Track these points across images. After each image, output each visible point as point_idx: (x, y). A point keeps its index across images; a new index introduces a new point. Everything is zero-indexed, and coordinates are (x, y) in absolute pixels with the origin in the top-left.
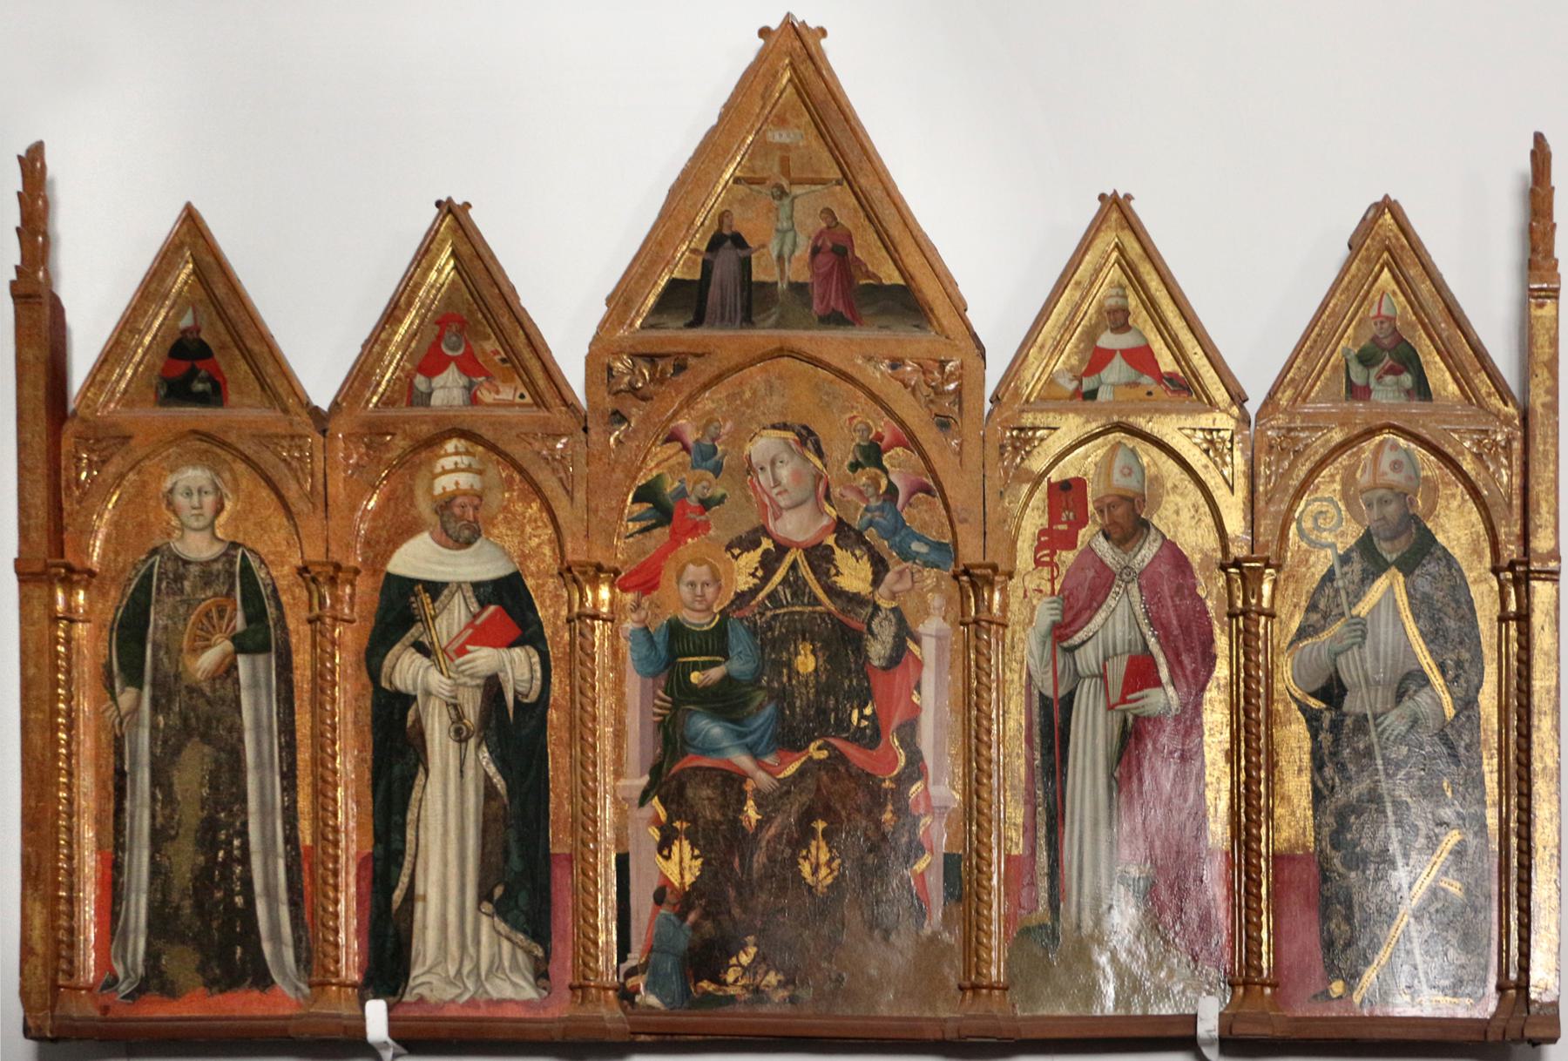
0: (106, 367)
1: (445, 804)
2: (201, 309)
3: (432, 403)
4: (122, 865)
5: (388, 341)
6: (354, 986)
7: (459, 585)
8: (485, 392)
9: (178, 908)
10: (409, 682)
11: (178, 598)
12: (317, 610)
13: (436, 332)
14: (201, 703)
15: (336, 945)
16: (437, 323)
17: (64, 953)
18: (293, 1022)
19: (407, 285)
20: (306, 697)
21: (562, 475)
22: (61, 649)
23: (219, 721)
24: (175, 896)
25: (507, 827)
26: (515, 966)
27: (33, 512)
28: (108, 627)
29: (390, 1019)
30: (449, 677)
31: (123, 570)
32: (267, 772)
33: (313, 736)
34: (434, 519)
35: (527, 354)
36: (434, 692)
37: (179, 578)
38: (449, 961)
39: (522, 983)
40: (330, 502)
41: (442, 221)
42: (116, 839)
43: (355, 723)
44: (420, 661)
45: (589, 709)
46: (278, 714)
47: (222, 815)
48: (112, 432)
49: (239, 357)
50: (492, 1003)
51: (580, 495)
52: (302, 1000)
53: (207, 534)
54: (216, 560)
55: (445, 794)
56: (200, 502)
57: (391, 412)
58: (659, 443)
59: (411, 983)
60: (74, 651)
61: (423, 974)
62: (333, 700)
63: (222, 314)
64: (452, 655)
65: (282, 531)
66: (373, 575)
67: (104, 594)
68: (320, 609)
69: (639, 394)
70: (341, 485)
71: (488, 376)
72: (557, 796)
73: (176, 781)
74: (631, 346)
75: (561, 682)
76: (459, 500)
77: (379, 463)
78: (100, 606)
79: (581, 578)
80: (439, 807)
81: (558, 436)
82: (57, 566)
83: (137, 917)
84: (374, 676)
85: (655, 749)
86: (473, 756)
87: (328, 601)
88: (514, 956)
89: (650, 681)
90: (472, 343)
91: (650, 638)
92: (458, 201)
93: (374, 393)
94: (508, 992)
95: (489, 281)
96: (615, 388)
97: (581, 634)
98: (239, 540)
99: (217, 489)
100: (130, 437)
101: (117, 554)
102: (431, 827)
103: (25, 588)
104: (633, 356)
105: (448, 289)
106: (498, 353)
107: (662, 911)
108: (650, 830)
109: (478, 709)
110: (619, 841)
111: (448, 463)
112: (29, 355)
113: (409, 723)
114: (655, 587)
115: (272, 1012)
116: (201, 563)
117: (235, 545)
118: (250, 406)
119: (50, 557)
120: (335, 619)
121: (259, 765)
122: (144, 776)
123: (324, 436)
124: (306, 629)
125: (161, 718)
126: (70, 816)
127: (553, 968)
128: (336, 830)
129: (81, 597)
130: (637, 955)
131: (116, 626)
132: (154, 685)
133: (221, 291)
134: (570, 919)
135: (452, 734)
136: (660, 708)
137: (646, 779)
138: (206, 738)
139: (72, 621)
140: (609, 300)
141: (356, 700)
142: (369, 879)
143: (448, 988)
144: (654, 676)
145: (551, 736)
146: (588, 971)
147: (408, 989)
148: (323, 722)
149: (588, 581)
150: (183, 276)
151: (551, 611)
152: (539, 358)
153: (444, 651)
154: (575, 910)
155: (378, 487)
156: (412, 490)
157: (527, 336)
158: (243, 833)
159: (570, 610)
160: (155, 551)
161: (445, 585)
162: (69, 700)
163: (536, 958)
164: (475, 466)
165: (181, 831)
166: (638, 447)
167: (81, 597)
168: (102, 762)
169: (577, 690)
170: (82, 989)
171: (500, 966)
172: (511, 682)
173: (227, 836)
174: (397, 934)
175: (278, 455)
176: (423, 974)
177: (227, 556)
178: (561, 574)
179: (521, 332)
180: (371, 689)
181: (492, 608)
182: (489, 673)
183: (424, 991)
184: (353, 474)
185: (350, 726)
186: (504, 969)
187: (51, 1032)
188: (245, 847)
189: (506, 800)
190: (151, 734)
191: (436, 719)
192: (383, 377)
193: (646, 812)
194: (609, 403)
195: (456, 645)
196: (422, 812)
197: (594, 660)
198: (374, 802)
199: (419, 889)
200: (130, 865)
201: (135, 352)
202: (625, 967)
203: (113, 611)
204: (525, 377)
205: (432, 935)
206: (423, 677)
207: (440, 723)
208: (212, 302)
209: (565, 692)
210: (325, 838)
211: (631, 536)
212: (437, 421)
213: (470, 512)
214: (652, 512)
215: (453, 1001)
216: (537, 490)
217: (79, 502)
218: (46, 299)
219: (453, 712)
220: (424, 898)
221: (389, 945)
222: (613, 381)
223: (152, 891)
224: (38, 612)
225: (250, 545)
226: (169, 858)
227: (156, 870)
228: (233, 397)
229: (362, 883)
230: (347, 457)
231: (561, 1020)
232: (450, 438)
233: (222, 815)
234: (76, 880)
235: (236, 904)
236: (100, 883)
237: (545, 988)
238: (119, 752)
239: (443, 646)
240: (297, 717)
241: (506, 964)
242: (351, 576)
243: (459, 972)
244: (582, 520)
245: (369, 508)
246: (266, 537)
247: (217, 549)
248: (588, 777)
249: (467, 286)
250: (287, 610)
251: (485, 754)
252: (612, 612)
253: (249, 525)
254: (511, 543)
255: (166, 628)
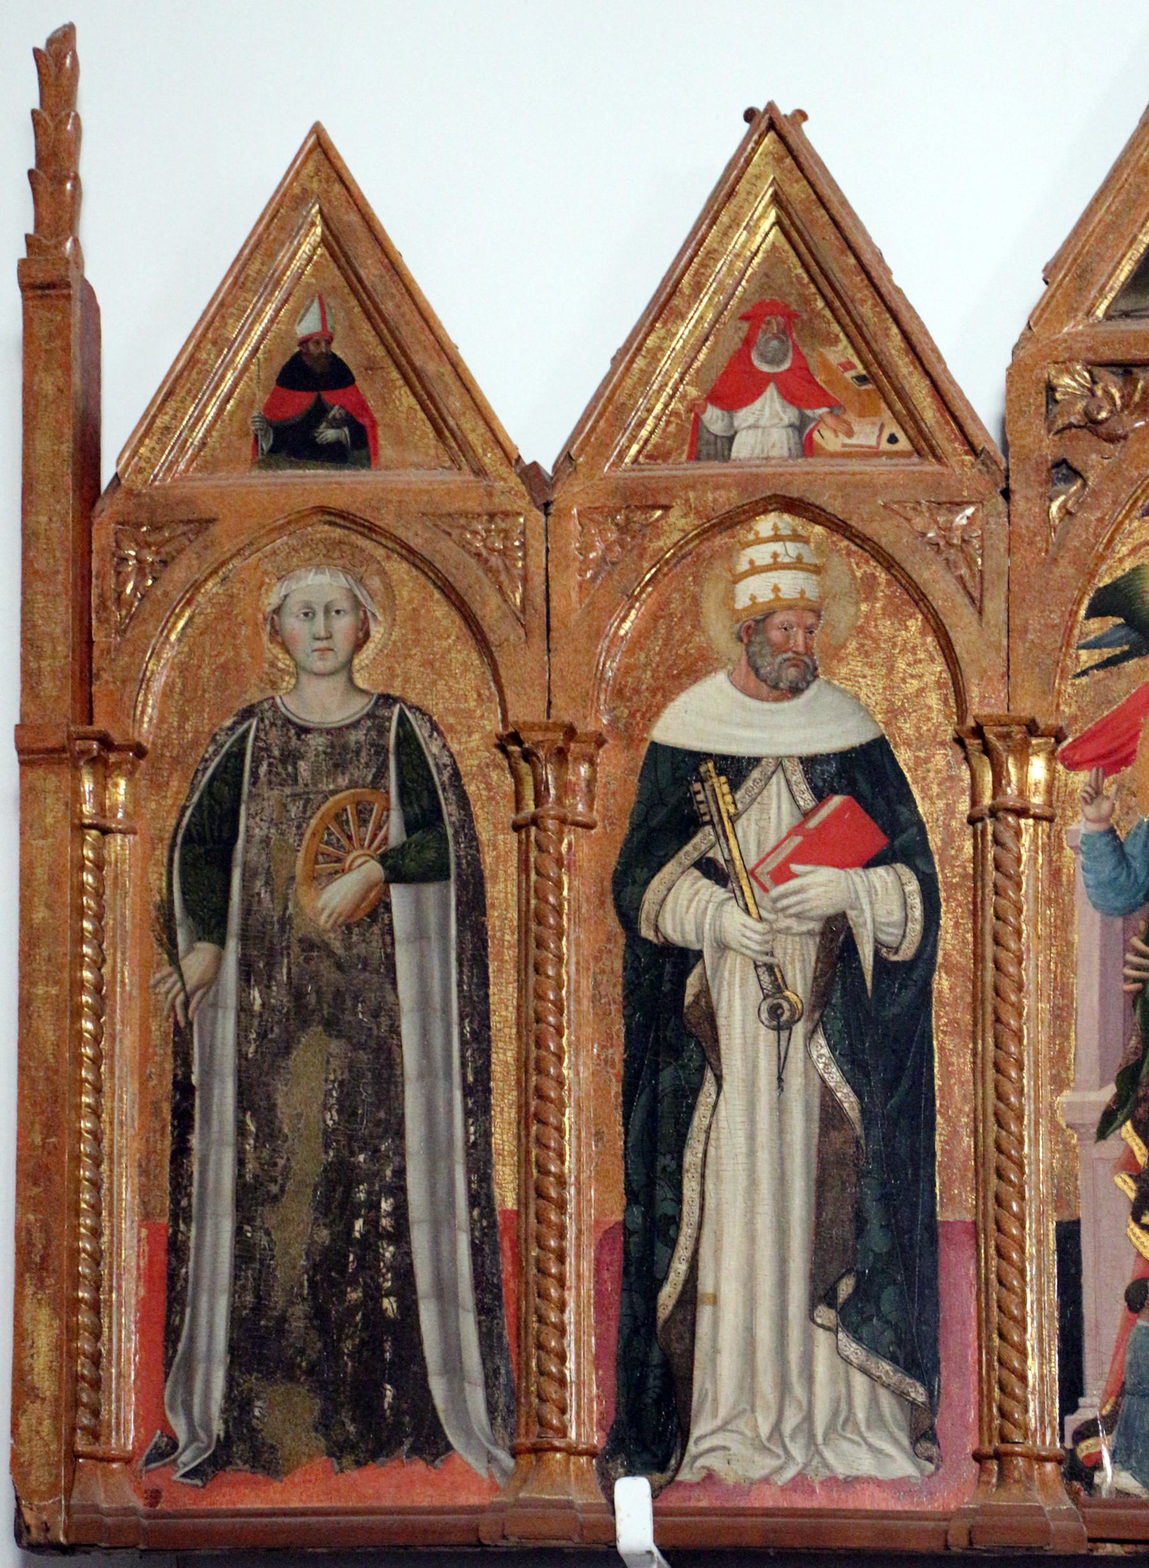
0: (172, 405)
1: (752, 1137)
2: (330, 301)
3: (734, 454)
4: (185, 1243)
5: (654, 357)
6: (591, 1453)
7: (779, 762)
8: (827, 433)
9: (283, 1319)
10: (690, 928)
11: (288, 791)
12: (530, 807)
13: (742, 335)
14: (325, 968)
15: (562, 1382)
16: (745, 318)
17: (85, 1398)
18: (489, 1516)
19: (695, 254)
20: (510, 954)
21: (964, 571)
22: (88, 878)
23: (356, 998)
24: (278, 1298)
25: (861, 1174)
26: (876, 1419)
27: (47, 647)
28: (167, 842)
29: (657, 1513)
30: (761, 919)
31: (195, 744)
32: (441, 1084)
33: (521, 1024)
34: (737, 651)
35: (903, 366)
36: (734, 945)
37: (290, 757)
38: (759, 1410)
39: (888, 1448)
40: (554, 623)
41: (758, 143)
42: (176, 1202)
43: (594, 999)
44: (708, 889)
45: (1012, 970)
46: (460, 984)
47: (361, 1158)
48: (183, 513)
49: (401, 382)
50: (832, 1482)
51: (995, 606)
52: (499, 1480)
53: (340, 680)
54: (355, 725)
55: (752, 1121)
56: (328, 627)
57: (661, 470)
58: (1136, 513)
59: (692, 1448)
60: (109, 883)
61: (713, 1432)
62: (559, 958)
63: (373, 313)
64: (767, 880)
65: (470, 675)
66: (628, 747)
67: (158, 786)
68: (537, 806)
69: (1102, 429)
70: (574, 595)
71: (833, 405)
72: (948, 1120)
73: (280, 1101)
74: (1089, 349)
75: (957, 925)
76: (779, 618)
77: (641, 556)
78: (153, 806)
79: (999, 745)
80: (741, 1140)
81: (958, 505)
82: (85, 737)
83: (211, 1336)
84: (628, 918)
85: (1127, 1038)
86: (801, 1055)
87: (552, 791)
88: (874, 1401)
89: (1119, 923)
90: (805, 351)
91: (1118, 848)
92: (786, 109)
93: (633, 439)
94: (866, 1465)
95: (837, 243)
96: (1060, 423)
97: (997, 841)
98: (396, 692)
99: (357, 604)
100: (212, 521)
101: (184, 717)
102: (726, 1175)
103: (31, 775)
104: (1093, 365)
105: (764, 260)
106: (853, 367)
107: (1141, 1322)
108: (1119, 1180)
109: (810, 974)
110: (1061, 1199)
111: (761, 554)
112: (48, 385)
113: (688, 999)
114: (1127, 761)
115: (446, 1501)
116: (329, 732)
117: (387, 700)
118: (418, 466)
119: (74, 722)
120: (563, 821)
121: (426, 1072)
122: (225, 1094)
123: (547, 514)
124: (510, 840)
125: (256, 994)
126: (97, 1163)
127: (944, 1423)
128: (561, 1182)
129: (120, 790)
130: (1097, 1401)
131: (179, 839)
132: (244, 938)
133: (370, 270)
134: (972, 1336)
135: (764, 1015)
136: (1138, 968)
137: (1109, 1092)
138: (332, 1026)
139: (105, 831)
140: (1050, 273)
141: (597, 959)
142: (617, 1267)
143: (757, 1457)
144: (1127, 913)
145: (940, 1019)
146: (1009, 1426)
147: (686, 1459)
148: (541, 997)
149: (1010, 750)
150: (306, 248)
151: (941, 804)
152: (927, 374)
153: (751, 874)
154: (983, 1323)
155: (637, 599)
156: (696, 600)
157: (905, 335)
158: (398, 1190)
159: (974, 802)
160: (248, 713)
161: (755, 761)
162: (98, 965)
163: (913, 1403)
164: (809, 558)
165: (290, 1186)
166: (1100, 520)
167: (120, 790)
168: (151, 1069)
169: (989, 939)
170: (113, 1460)
171: (850, 1418)
172: (870, 926)
173: (369, 1193)
174: (666, 1362)
175: (464, 545)
176: (713, 1432)
177: (374, 720)
178: (959, 741)
179: (895, 330)
180: (622, 941)
181: (837, 800)
182: (831, 911)
183: (714, 1462)
184: (594, 578)
185: (585, 1003)
186: (856, 1425)
187: (66, 1535)
188: (401, 1212)
189: (859, 1130)
190: (238, 1022)
191: (737, 989)
192: (649, 411)
193: (1111, 1148)
194: (1048, 448)
195: (772, 864)
196: (712, 1151)
197: (1019, 886)
198: (627, 1133)
199: (706, 1284)
200: (199, 1248)
201: (223, 377)
202: (1073, 1421)
203: (175, 814)
204: (898, 406)
205: (728, 1365)
206: (714, 918)
207: (743, 998)
208: (353, 290)
209: (964, 942)
210: (541, 1194)
211: (1084, 673)
212: (746, 482)
213: (799, 637)
214: (1123, 632)
215: (766, 1480)
216: (918, 597)
217: (121, 632)
218: (76, 291)
219: (766, 978)
220: (715, 1300)
221: (652, 1382)
222: (1056, 409)
223: (236, 1291)
224: (53, 813)
225: (413, 698)
226: (268, 1233)
227: (244, 1252)
228: (386, 450)
229: (606, 1275)
230: (585, 549)
231: (961, 1513)
232: (765, 512)
233: (361, 1158)
234: (105, 1272)
235: (383, 1312)
236: (147, 1277)
237: (929, 1459)
238: (182, 1054)
239: (749, 867)
240: (492, 990)
241: (861, 1415)
242: (590, 749)
243: (777, 1428)
244: (998, 650)
245: (622, 632)
246: (441, 685)
247: (358, 706)
248: (1008, 1087)
249: (799, 255)
250: (477, 810)
251: (821, 1049)
252: (1049, 803)
253: (414, 667)
254: (871, 690)
255: (266, 841)
